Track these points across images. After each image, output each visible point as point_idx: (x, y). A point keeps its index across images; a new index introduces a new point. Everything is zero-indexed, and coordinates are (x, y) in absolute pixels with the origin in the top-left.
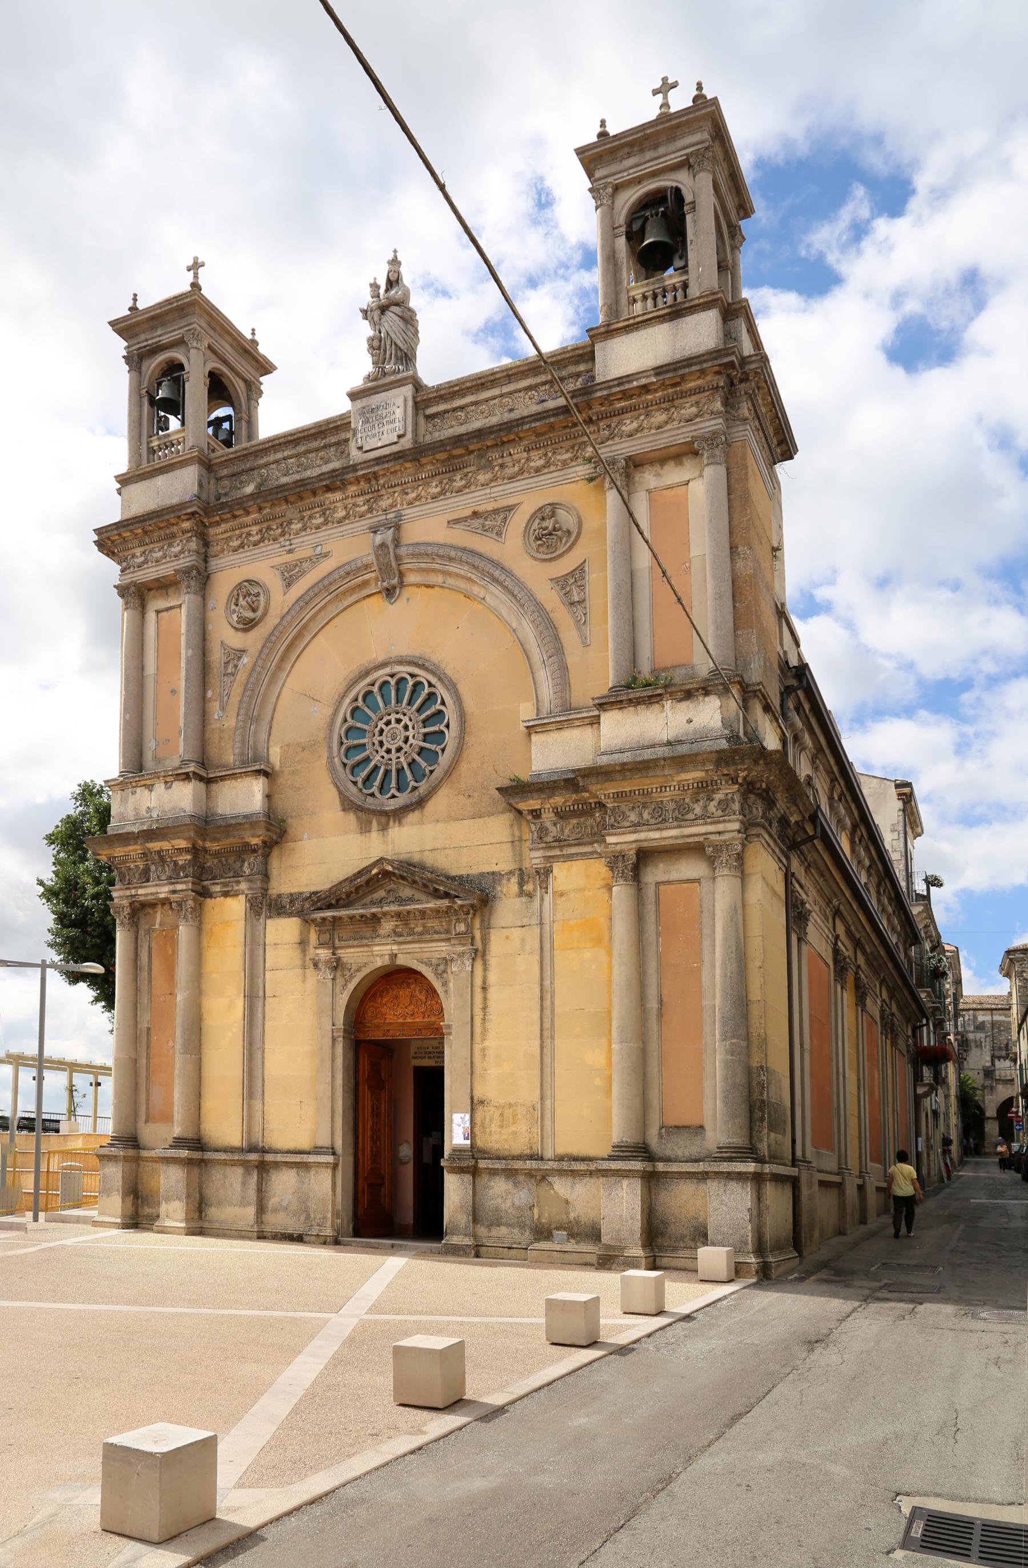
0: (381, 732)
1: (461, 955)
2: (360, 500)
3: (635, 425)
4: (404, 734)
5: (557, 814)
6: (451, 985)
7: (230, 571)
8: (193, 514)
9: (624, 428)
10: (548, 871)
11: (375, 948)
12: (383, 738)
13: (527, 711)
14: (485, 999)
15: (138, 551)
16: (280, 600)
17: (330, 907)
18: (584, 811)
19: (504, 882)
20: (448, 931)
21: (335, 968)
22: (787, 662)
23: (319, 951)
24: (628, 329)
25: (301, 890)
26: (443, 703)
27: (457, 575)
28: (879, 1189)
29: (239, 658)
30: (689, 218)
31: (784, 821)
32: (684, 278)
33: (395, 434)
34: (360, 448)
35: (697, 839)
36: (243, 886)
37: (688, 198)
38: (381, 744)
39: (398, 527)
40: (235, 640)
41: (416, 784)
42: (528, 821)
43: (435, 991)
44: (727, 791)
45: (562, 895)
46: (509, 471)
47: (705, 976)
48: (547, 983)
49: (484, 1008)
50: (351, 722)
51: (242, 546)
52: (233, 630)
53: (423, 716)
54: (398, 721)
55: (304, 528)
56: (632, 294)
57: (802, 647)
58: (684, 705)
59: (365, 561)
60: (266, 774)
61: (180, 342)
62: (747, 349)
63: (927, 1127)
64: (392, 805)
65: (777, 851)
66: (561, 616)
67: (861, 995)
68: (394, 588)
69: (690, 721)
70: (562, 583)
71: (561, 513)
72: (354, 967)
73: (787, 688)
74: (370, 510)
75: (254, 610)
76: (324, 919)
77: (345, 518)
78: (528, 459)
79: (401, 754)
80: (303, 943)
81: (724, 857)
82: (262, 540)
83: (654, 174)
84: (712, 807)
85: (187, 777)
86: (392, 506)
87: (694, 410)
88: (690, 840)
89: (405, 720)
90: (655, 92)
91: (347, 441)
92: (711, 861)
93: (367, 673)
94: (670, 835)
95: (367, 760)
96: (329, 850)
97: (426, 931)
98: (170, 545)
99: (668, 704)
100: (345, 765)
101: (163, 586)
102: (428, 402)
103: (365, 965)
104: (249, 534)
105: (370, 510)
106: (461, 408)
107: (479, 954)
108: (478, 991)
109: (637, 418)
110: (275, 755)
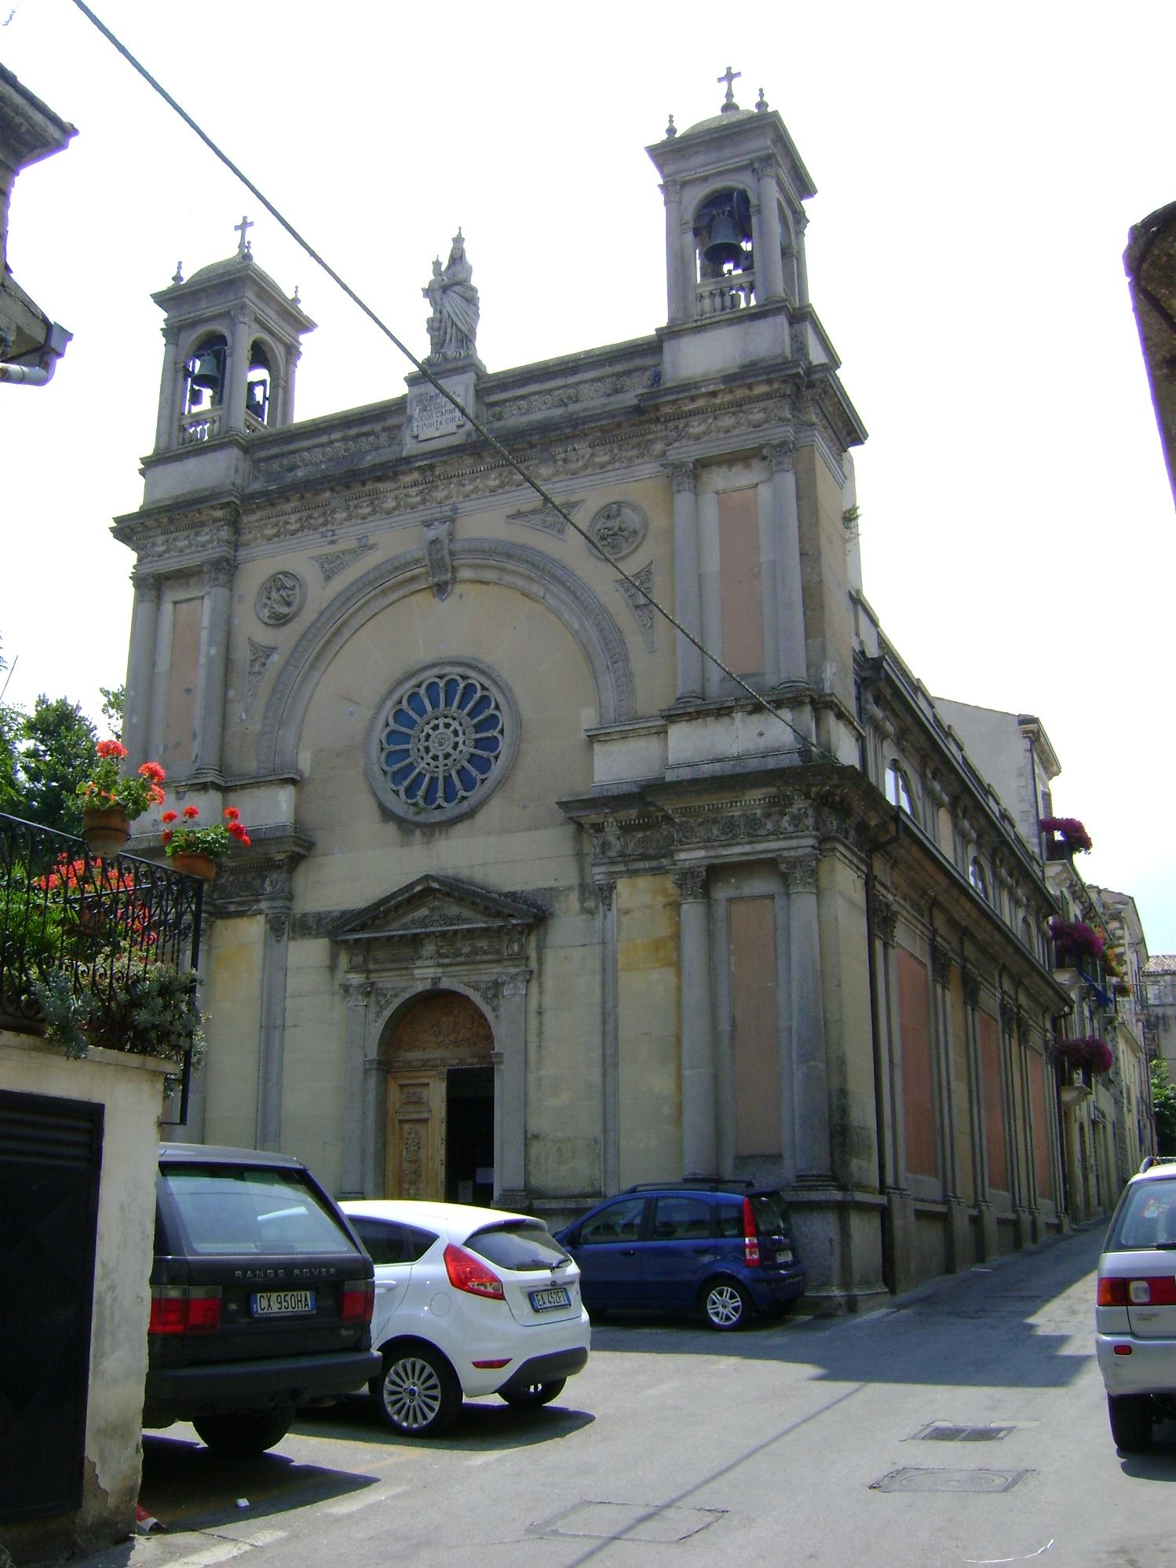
0: (428, 736)
1: (513, 977)
2: (413, 491)
3: (702, 428)
4: (454, 739)
5: (621, 828)
6: (502, 1010)
7: (261, 563)
8: (228, 503)
9: (691, 430)
10: (612, 887)
11: (416, 972)
12: (430, 744)
13: (588, 718)
14: (541, 1024)
15: (160, 539)
16: (318, 595)
17: (363, 927)
18: (648, 823)
19: (563, 898)
20: (499, 952)
21: (368, 994)
22: (863, 653)
23: (350, 976)
24: (699, 329)
25: (330, 909)
26: (497, 707)
27: (515, 573)
28: (1001, 1222)
29: (268, 656)
30: (754, 220)
31: (862, 828)
32: (751, 279)
33: (454, 425)
34: (416, 437)
35: (770, 855)
36: (264, 905)
37: (753, 201)
38: (427, 750)
39: (453, 520)
40: (265, 636)
41: (465, 794)
42: (590, 835)
43: (482, 1016)
44: (799, 805)
45: (627, 913)
46: (572, 466)
47: (781, 996)
48: (609, 1005)
49: (540, 1034)
50: (393, 726)
51: (277, 535)
52: (263, 626)
53: (476, 721)
54: (447, 726)
55: (349, 518)
56: (699, 291)
57: (881, 624)
58: (755, 717)
59: (416, 555)
60: (293, 781)
61: (226, 315)
62: (817, 356)
63: (1083, 1142)
64: (436, 817)
65: (855, 861)
66: (626, 619)
67: (970, 994)
68: (446, 583)
69: (761, 734)
70: (627, 583)
71: (626, 511)
72: (390, 993)
73: (864, 679)
74: (424, 501)
75: (289, 604)
76: (356, 940)
77: (395, 509)
78: (592, 455)
79: (449, 762)
80: (333, 967)
81: (798, 874)
82: (301, 529)
83: (720, 174)
84: (785, 822)
85: (204, 787)
86: (447, 498)
87: (761, 415)
88: (762, 856)
89: (455, 725)
90: (720, 80)
91: (399, 427)
92: (785, 879)
93: (413, 675)
94: (736, 852)
95: (411, 767)
96: (361, 867)
97: (475, 951)
98: (197, 534)
99: (738, 716)
100: (385, 772)
101: (182, 576)
102: (489, 391)
103: (404, 990)
104: (287, 523)
105: (424, 501)
106: (523, 397)
107: (535, 975)
108: (532, 1015)
109: (705, 421)
110: (305, 762)
